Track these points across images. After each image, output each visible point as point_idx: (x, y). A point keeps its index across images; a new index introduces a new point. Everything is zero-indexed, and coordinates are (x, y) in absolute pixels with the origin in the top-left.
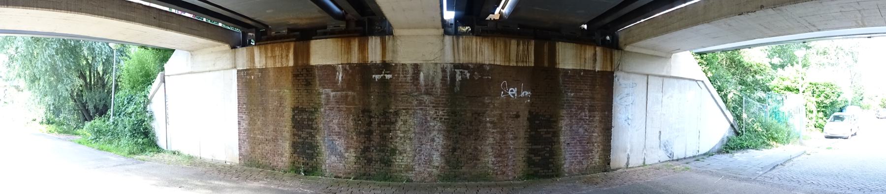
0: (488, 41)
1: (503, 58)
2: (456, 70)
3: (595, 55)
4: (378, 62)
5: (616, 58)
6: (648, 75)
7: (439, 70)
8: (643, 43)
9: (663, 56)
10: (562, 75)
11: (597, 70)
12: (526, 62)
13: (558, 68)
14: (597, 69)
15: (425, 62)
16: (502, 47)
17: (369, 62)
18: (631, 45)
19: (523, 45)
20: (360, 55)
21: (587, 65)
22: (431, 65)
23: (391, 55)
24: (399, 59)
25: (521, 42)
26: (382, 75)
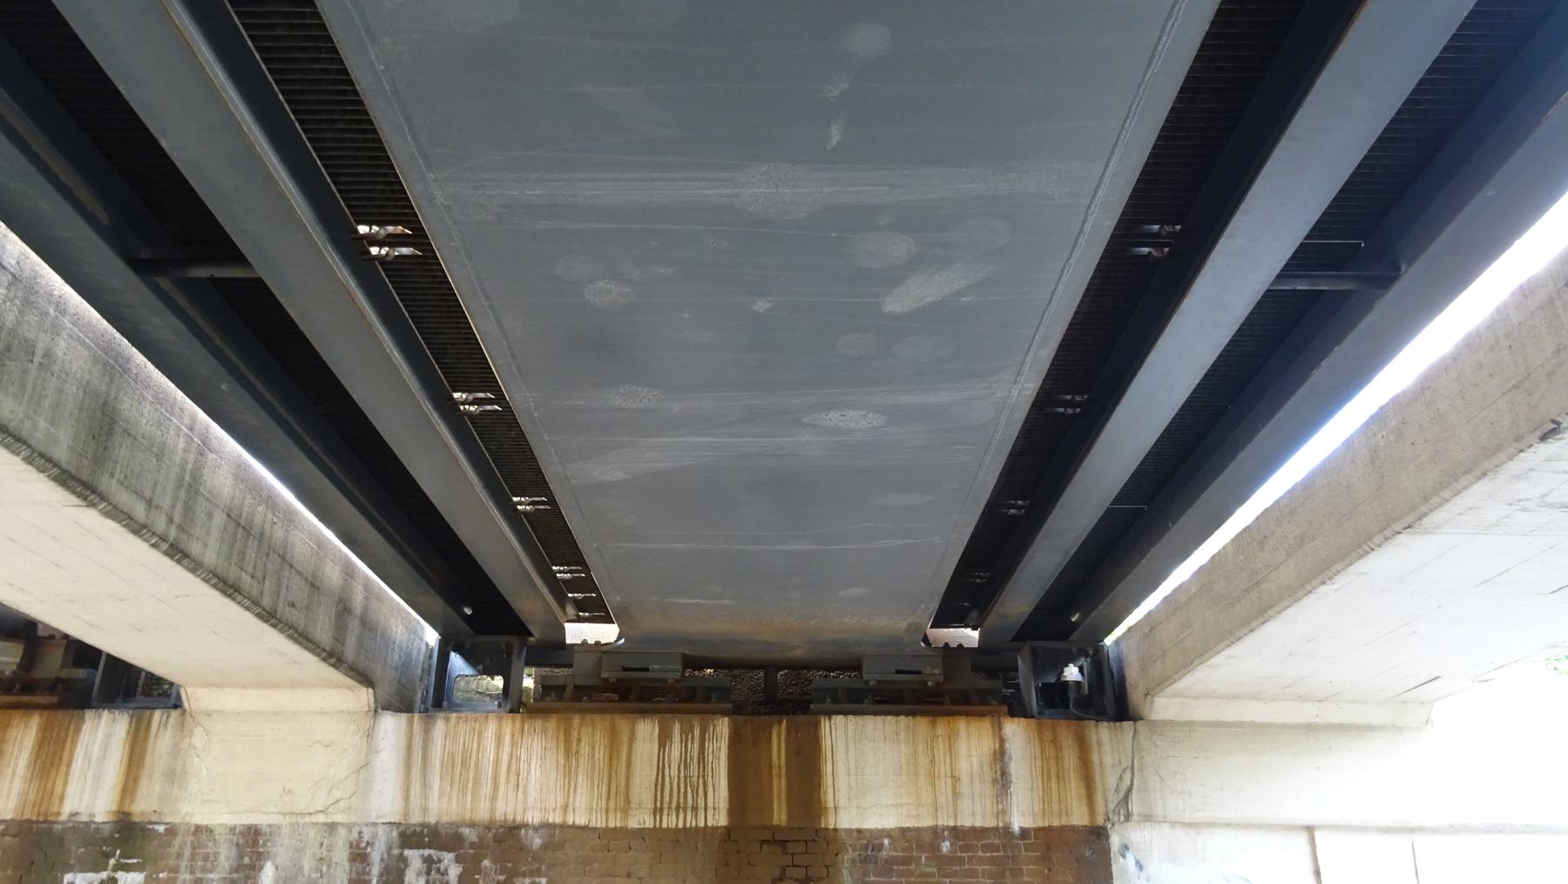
0: (545, 732)
1: (600, 795)
2: (407, 852)
3: (1000, 755)
4: (99, 819)
5: (1108, 760)
6: (1310, 830)
7: (341, 855)
8: (1201, 677)
9: (1375, 722)
10: (853, 861)
11: (1016, 827)
12: (695, 809)
13: (835, 830)
14: (1018, 822)
15: (288, 819)
16: (601, 752)
17: (63, 817)
18: (1168, 691)
19: (684, 742)
20: (35, 784)
21: (965, 804)
22: (312, 833)
23: (157, 788)
24: (185, 808)
25: (677, 728)
26: (104, 875)
